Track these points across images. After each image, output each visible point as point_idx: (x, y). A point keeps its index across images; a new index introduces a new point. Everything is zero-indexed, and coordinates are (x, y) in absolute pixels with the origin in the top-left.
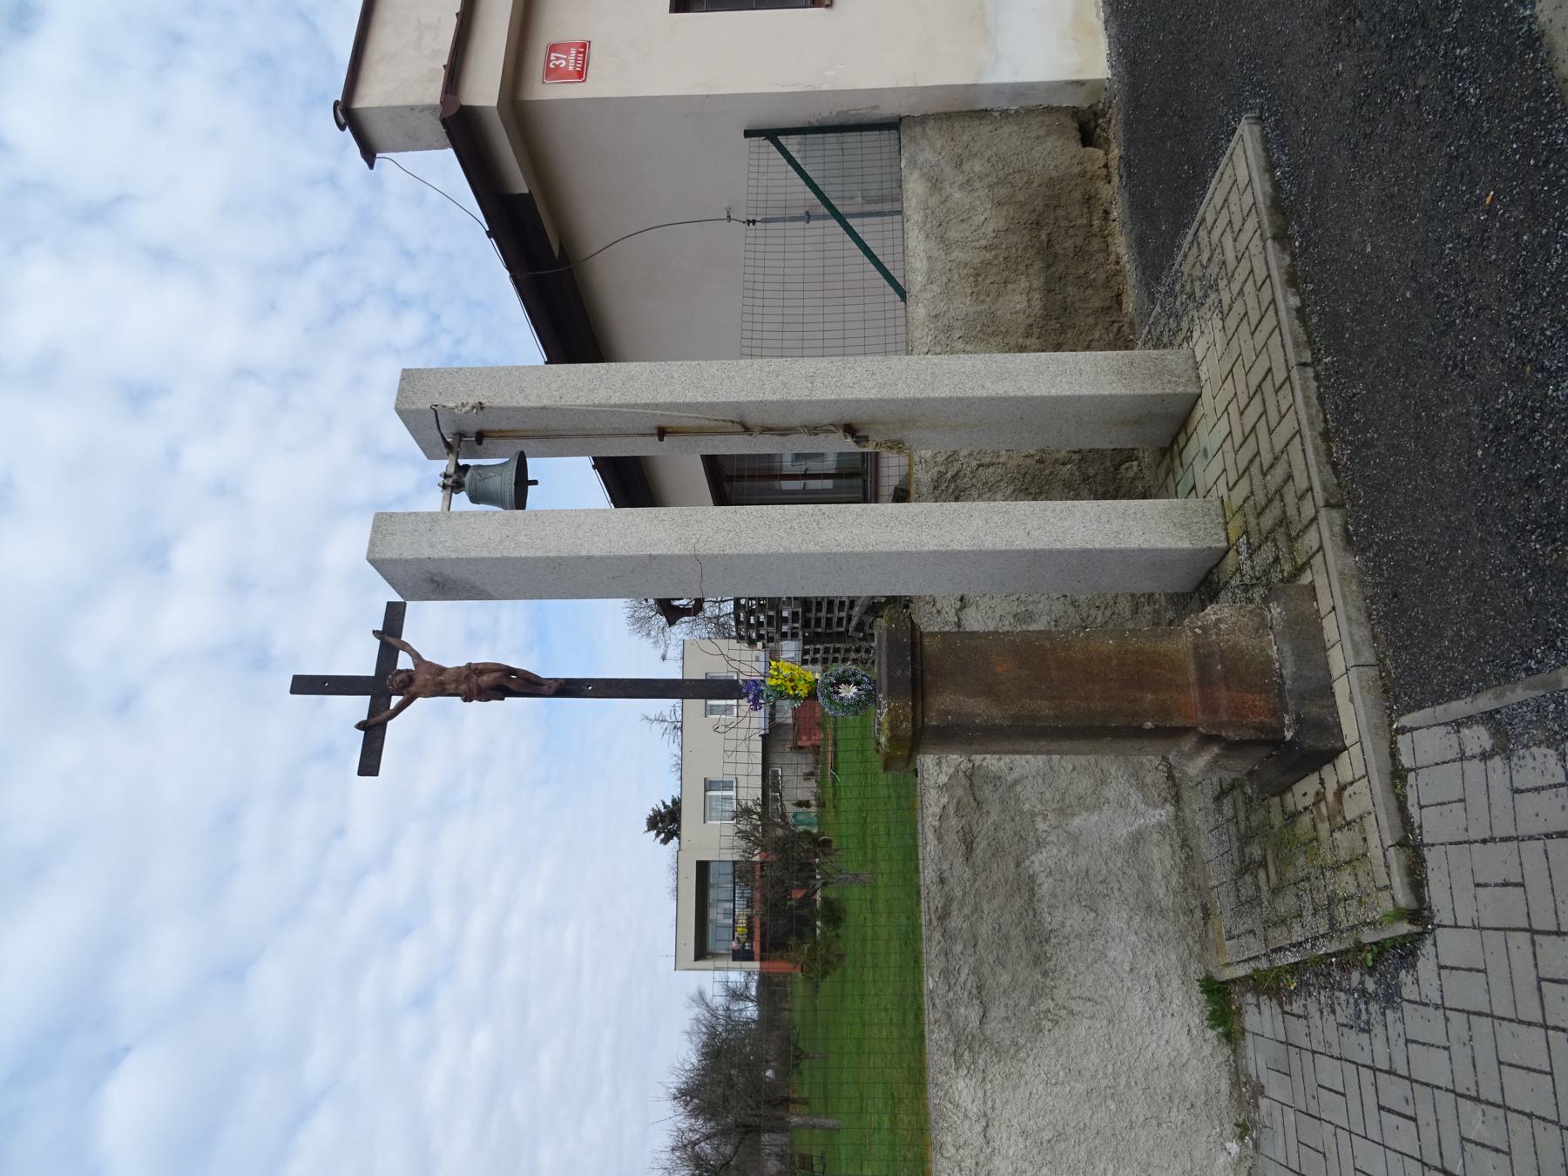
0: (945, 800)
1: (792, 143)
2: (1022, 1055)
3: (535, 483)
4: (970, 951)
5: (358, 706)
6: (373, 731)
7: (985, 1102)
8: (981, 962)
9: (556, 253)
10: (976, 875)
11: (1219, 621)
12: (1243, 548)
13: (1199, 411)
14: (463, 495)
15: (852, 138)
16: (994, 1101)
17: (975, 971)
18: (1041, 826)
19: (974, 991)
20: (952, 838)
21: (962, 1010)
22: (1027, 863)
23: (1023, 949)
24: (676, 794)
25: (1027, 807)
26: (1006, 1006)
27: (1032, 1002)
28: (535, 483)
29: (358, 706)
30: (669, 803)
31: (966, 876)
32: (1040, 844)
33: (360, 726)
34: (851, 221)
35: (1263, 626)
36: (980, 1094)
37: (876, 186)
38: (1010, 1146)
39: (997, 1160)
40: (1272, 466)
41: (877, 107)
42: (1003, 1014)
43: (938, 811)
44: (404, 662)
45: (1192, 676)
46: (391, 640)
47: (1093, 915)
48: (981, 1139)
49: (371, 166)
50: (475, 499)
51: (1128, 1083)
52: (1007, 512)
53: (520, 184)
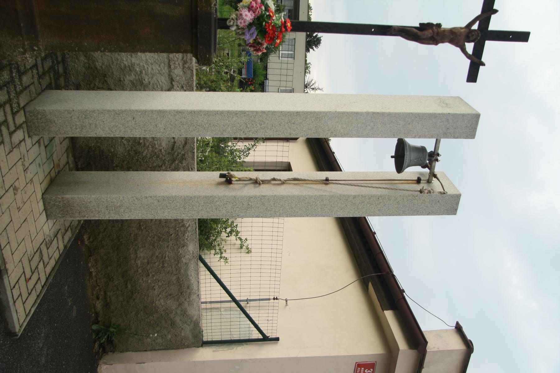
1: (256, 335)
3: (392, 157)
5: (495, 24)
9: (370, 285)
11: (24, 53)
12: (15, 106)
13: (45, 185)
14: (429, 151)
15: (226, 337)
24: (308, 54)
28: (392, 157)
29: (495, 24)
30: (311, 50)
33: (496, 11)
34: (229, 299)
37: (214, 317)
41: (214, 351)
44: (470, 47)
46: (476, 60)
49: (457, 323)
50: (423, 149)
53: (389, 315)
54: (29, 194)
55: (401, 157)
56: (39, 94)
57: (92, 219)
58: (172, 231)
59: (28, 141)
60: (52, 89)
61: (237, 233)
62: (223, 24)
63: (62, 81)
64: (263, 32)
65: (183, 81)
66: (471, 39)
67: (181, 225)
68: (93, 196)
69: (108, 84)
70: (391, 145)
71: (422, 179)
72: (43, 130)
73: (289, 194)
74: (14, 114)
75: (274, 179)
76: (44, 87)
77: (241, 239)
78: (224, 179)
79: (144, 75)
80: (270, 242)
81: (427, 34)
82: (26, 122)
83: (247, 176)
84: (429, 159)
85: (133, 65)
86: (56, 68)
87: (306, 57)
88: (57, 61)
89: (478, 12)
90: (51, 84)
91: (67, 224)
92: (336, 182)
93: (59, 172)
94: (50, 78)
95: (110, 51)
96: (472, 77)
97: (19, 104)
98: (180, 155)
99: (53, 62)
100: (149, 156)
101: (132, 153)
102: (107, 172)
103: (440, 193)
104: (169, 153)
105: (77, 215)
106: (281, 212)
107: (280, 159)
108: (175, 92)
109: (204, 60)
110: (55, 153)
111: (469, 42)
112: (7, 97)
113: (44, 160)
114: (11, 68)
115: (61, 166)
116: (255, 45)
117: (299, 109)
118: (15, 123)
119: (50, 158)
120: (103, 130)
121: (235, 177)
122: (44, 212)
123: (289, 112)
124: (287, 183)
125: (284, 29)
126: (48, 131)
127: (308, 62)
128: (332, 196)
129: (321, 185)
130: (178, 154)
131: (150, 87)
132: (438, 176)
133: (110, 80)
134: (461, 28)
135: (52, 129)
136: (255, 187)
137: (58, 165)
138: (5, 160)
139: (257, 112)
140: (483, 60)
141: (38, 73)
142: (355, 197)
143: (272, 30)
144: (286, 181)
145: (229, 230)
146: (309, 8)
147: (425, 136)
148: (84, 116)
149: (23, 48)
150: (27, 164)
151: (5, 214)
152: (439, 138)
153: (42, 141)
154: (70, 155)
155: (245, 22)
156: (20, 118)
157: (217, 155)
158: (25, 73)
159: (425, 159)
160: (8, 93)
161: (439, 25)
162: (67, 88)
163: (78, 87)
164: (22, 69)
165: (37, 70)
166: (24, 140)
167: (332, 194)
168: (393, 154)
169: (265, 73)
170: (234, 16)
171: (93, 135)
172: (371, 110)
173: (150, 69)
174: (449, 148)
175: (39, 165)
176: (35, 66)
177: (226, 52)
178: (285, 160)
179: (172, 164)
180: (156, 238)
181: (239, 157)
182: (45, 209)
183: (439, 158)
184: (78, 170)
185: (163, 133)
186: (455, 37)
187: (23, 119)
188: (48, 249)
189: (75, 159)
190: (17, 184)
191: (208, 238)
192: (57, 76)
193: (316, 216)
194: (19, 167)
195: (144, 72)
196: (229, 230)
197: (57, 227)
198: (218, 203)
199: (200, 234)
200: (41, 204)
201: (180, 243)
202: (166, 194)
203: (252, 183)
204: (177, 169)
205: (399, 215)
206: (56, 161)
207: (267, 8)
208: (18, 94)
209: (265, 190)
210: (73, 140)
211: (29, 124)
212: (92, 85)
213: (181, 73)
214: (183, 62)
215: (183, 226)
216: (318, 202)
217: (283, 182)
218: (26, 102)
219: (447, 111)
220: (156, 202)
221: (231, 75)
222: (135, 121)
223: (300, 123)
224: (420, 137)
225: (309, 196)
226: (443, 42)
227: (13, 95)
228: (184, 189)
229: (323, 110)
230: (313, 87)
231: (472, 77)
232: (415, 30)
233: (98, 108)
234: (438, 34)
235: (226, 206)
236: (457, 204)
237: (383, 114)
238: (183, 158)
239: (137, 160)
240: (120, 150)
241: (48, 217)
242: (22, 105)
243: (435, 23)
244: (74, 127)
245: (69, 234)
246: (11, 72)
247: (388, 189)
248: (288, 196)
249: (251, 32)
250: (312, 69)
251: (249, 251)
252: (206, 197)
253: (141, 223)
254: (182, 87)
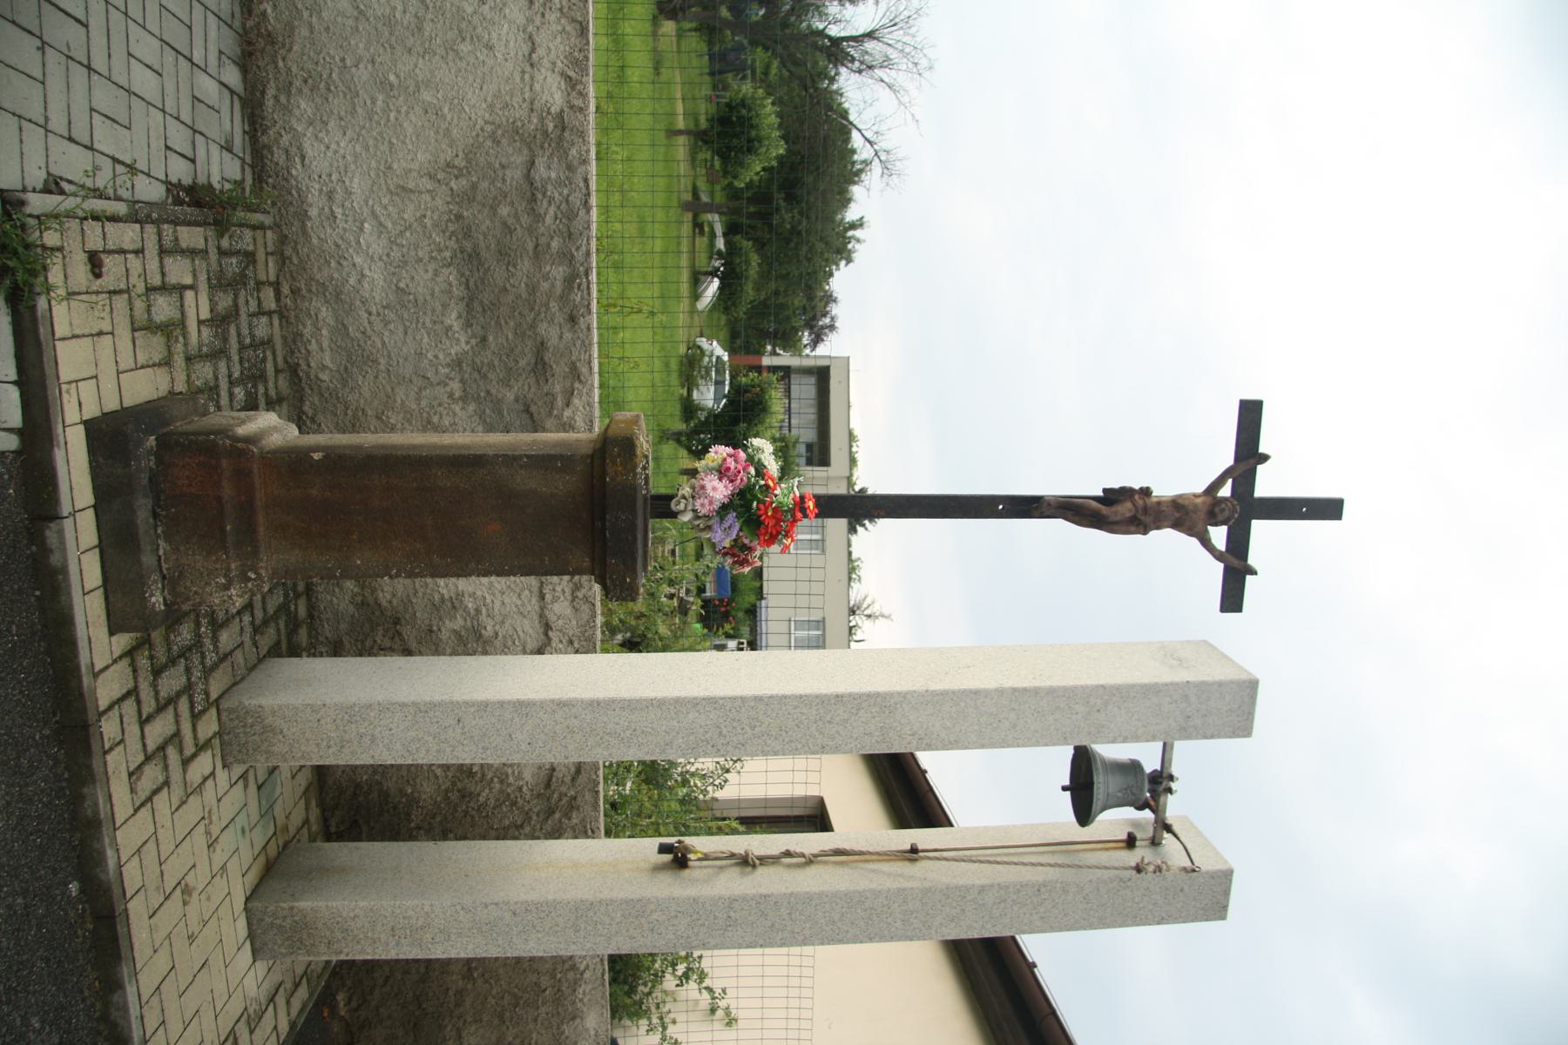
0: (568, 413)
2: (489, 128)
3: (1064, 789)
4: (543, 240)
5: (1267, 484)
6: (1249, 453)
7: (532, 78)
8: (530, 230)
10: (533, 326)
11: (227, 587)
12: (198, 698)
13: (252, 878)
14: (1148, 769)
16: (522, 79)
17: (539, 218)
18: (455, 386)
19: (539, 196)
20: (560, 368)
21: (553, 175)
22: (473, 341)
23: (482, 245)
24: (854, 538)
25: (472, 407)
26: (504, 180)
27: (474, 187)
31: (545, 325)
32: (457, 363)
33: (1264, 458)
35: (171, 582)
36: (537, 87)
38: (507, 37)
39: (521, 20)
40: (156, 791)
42: (508, 173)
43: (576, 401)
44: (1219, 535)
45: (261, 518)
46: (1235, 562)
47: (402, 285)
48: (538, 40)
50: (1134, 767)
51: (374, 102)
52: (485, 749)
54: (216, 900)
55: (1083, 788)
56: (252, 669)
57: (358, 957)
58: (545, 981)
59: (222, 775)
60: (280, 655)
61: (702, 976)
62: (663, 506)
63: (303, 636)
64: (753, 523)
65: (573, 629)
66: (1220, 518)
67: (567, 966)
68: (361, 904)
69: (403, 640)
70: (1059, 763)
71: (1138, 836)
73: (826, 888)
74: (195, 717)
75: (788, 854)
76: (263, 652)
77: (709, 989)
78: (668, 857)
79: (483, 617)
80: (783, 992)
81: (1120, 511)
82: (219, 734)
83: (724, 849)
84: (1152, 788)
85: (460, 595)
86: (293, 608)
87: (849, 545)
88: (295, 592)
89: (1228, 460)
90: (278, 643)
91: (299, 970)
92: (938, 854)
93: (286, 845)
94: (278, 630)
95: (411, 575)
96: (1232, 599)
97: (207, 694)
98: (565, 800)
99: (286, 595)
100: (492, 802)
101: (454, 796)
102: (395, 844)
103: (1184, 869)
104: (539, 795)
105: (323, 948)
106: (807, 932)
107: (800, 791)
108: (554, 656)
109: (619, 587)
110: (280, 801)
111: (1216, 524)
112: (184, 679)
113: (255, 817)
114: (198, 616)
115: (292, 830)
116: (736, 550)
117: (841, 689)
118: (195, 737)
119: (267, 813)
121: (696, 852)
122: (248, 943)
123: (817, 697)
124: (820, 862)
125: (799, 515)
126: (268, 752)
127: (854, 556)
128: (929, 890)
129: (900, 864)
130: (562, 795)
131: (498, 643)
132: (1175, 828)
133: (407, 631)
134: (1196, 496)
135: (275, 749)
136: (743, 874)
137: (286, 828)
138: (169, 824)
139: (743, 699)
140: (1252, 561)
141: (252, 623)
142: (982, 889)
143: (773, 517)
144: (815, 856)
145: (681, 968)
146: (851, 437)
147: (1137, 738)
149: (225, 576)
150: (215, 830)
151: (161, 952)
152: (1169, 740)
153: (251, 773)
154: (313, 803)
155: (711, 503)
156: (209, 725)
157: (652, 798)
158: (225, 624)
159: (1142, 790)
160: (188, 670)
161: (1146, 492)
162: (313, 651)
163: (337, 650)
164: (221, 616)
165: (253, 615)
166: (213, 774)
167: (927, 884)
168: (1067, 782)
169: (757, 584)
170: (687, 490)
171: (365, 759)
172: (1009, 683)
173: (497, 604)
174: (1194, 762)
175: (243, 831)
176: (249, 606)
177: (669, 547)
178: (813, 791)
179: (546, 819)
180: (507, 998)
181: (705, 792)
182: (251, 936)
183: (1174, 785)
184: (329, 838)
185: (525, 753)
186: (1184, 516)
187: (215, 727)
188: (251, 1032)
189: (323, 811)
190: (190, 879)
191: (632, 990)
192: (294, 625)
193: (892, 939)
194: (199, 838)
195: (484, 611)
196: (681, 968)
197: (276, 977)
198: (655, 916)
199: (613, 981)
200: (242, 923)
201: (564, 1010)
202: (533, 896)
203: (737, 864)
204: (556, 834)
205: (1091, 927)
206: (281, 821)
207: (761, 471)
208: (208, 672)
209: (767, 881)
210: (321, 772)
212: (368, 643)
213: (569, 611)
214: (572, 597)
215: (574, 968)
217: (810, 861)
218: (223, 687)
219: (1181, 676)
220: (508, 915)
221: (681, 600)
223: (846, 721)
224: (1125, 740)
225: (873, 891)
226: (1158, 528)
227: (197, 674)
228: (575, 882)
229: (898, 689)
230: (867, 612)
231: (1232, 599)
232: (1094, 504)
233: (380, 698)
234: (1146, 510)
235: (676, 922)
236: (1227, 893)
237: (1036, 691)
238: (572, 806)
239: (466, 813)
240: (427, 790)
241: (255, 953)
242: (214, 696)
243: (1137, 487)
245: (303, 993)
246: (198, 625)
247: (1060, 866)
248: (821, 895)
249: (726, 525)
250: (864, 571)
251: (731, 1021)
252: (627, 902)
253: (470, 966)
254: (571, 642)
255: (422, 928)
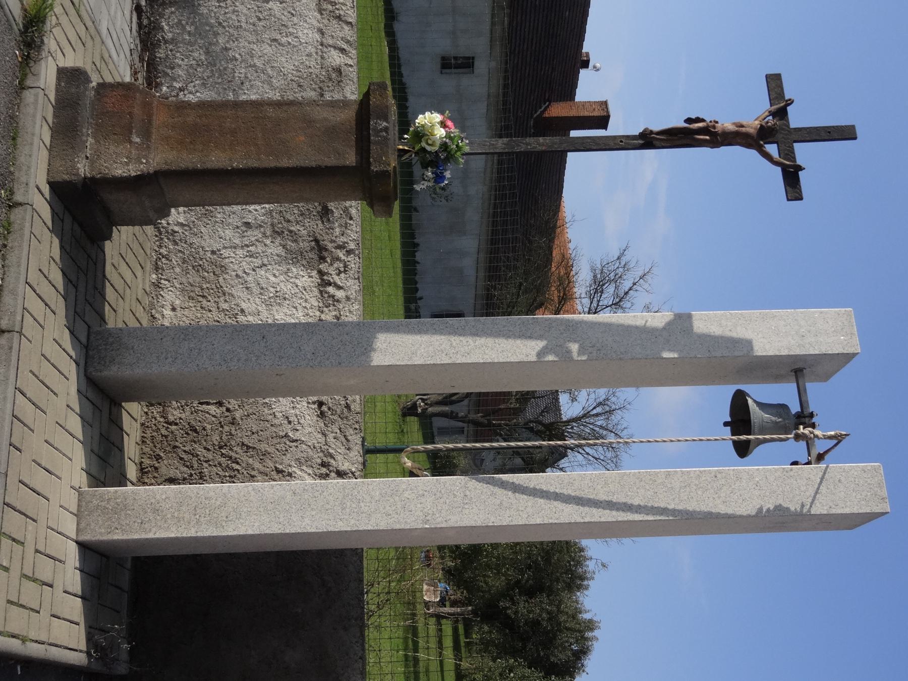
3: (726, 424)
72: (110, 362)
120: (210, 359)
148: (182, 336)
211: (91, 353)
216: (599, 487)
222: (266, 342)
235: (423, 500)
244: (164, 355)
255: (220, 507)
